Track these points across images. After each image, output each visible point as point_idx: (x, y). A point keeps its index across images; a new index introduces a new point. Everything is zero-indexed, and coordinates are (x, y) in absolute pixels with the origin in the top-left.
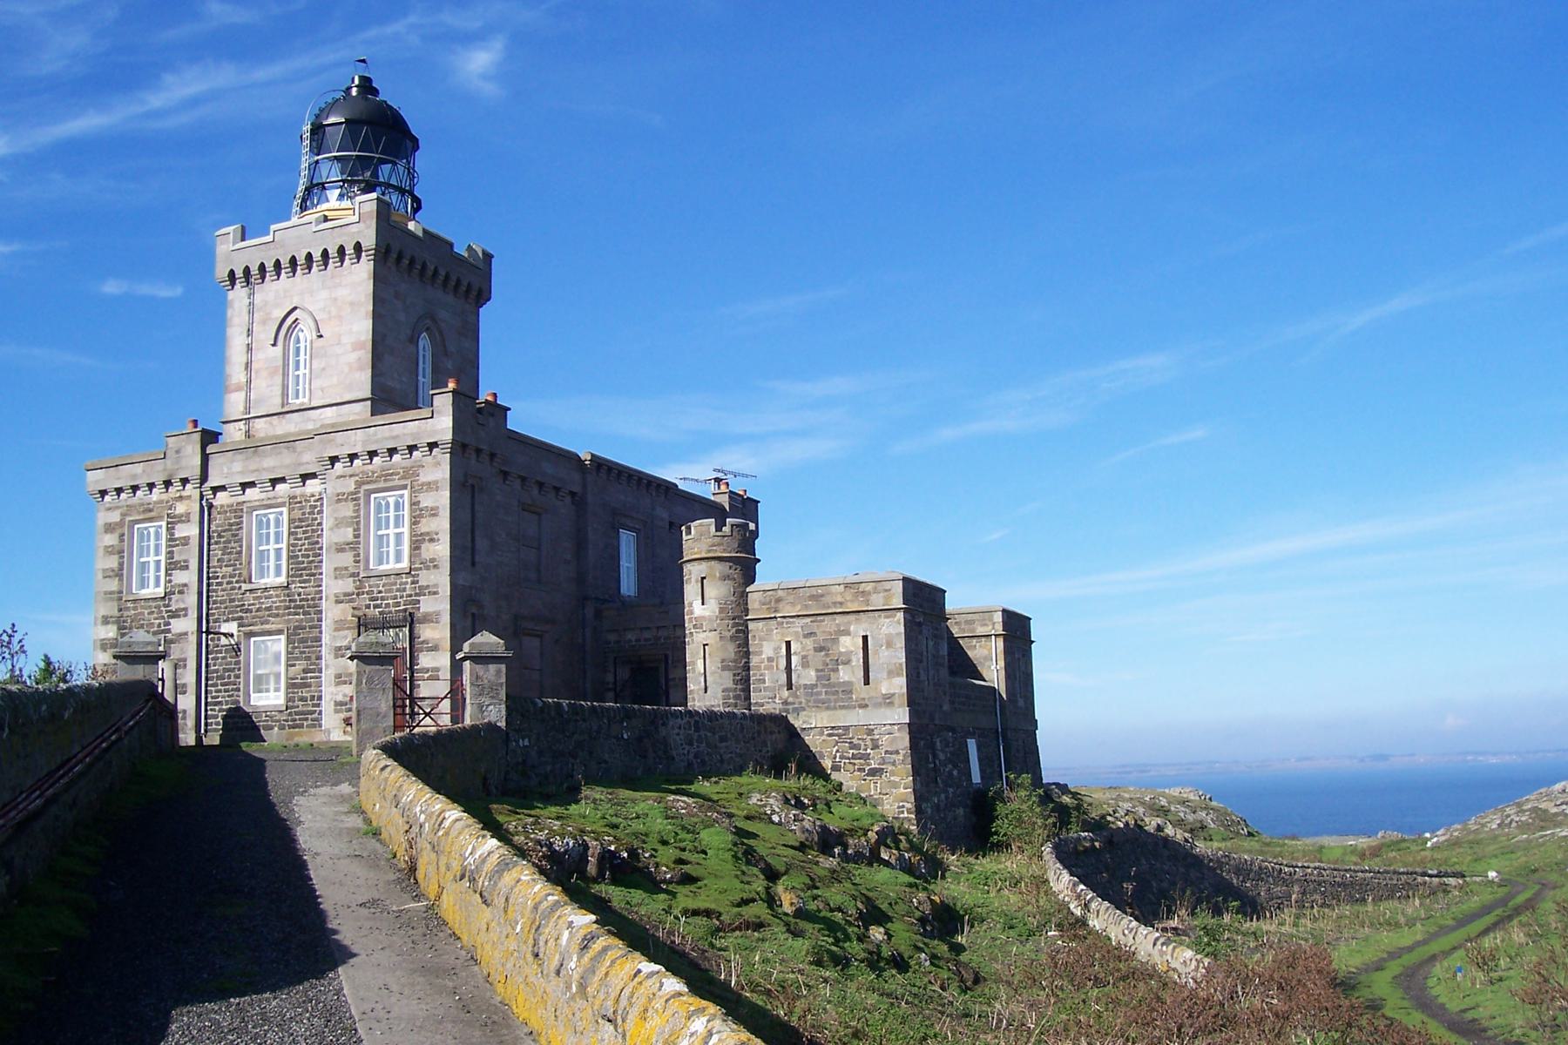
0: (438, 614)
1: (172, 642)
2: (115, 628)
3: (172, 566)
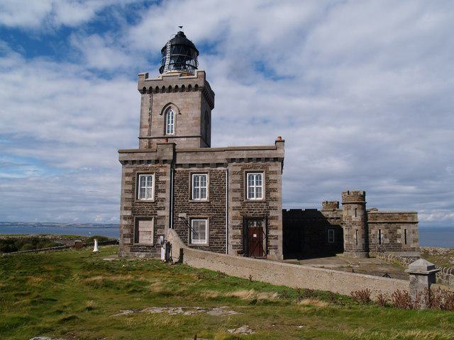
0: (277, 217)
1: (158, 219)
2: (131, 212)
3: (157, 191)
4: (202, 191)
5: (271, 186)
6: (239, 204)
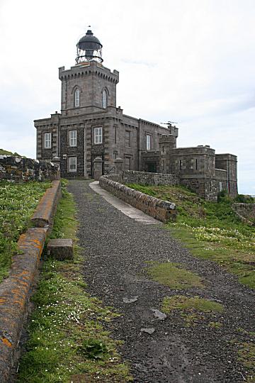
4: (73, 141)
5: (105, 135)
6: (90, 147)
